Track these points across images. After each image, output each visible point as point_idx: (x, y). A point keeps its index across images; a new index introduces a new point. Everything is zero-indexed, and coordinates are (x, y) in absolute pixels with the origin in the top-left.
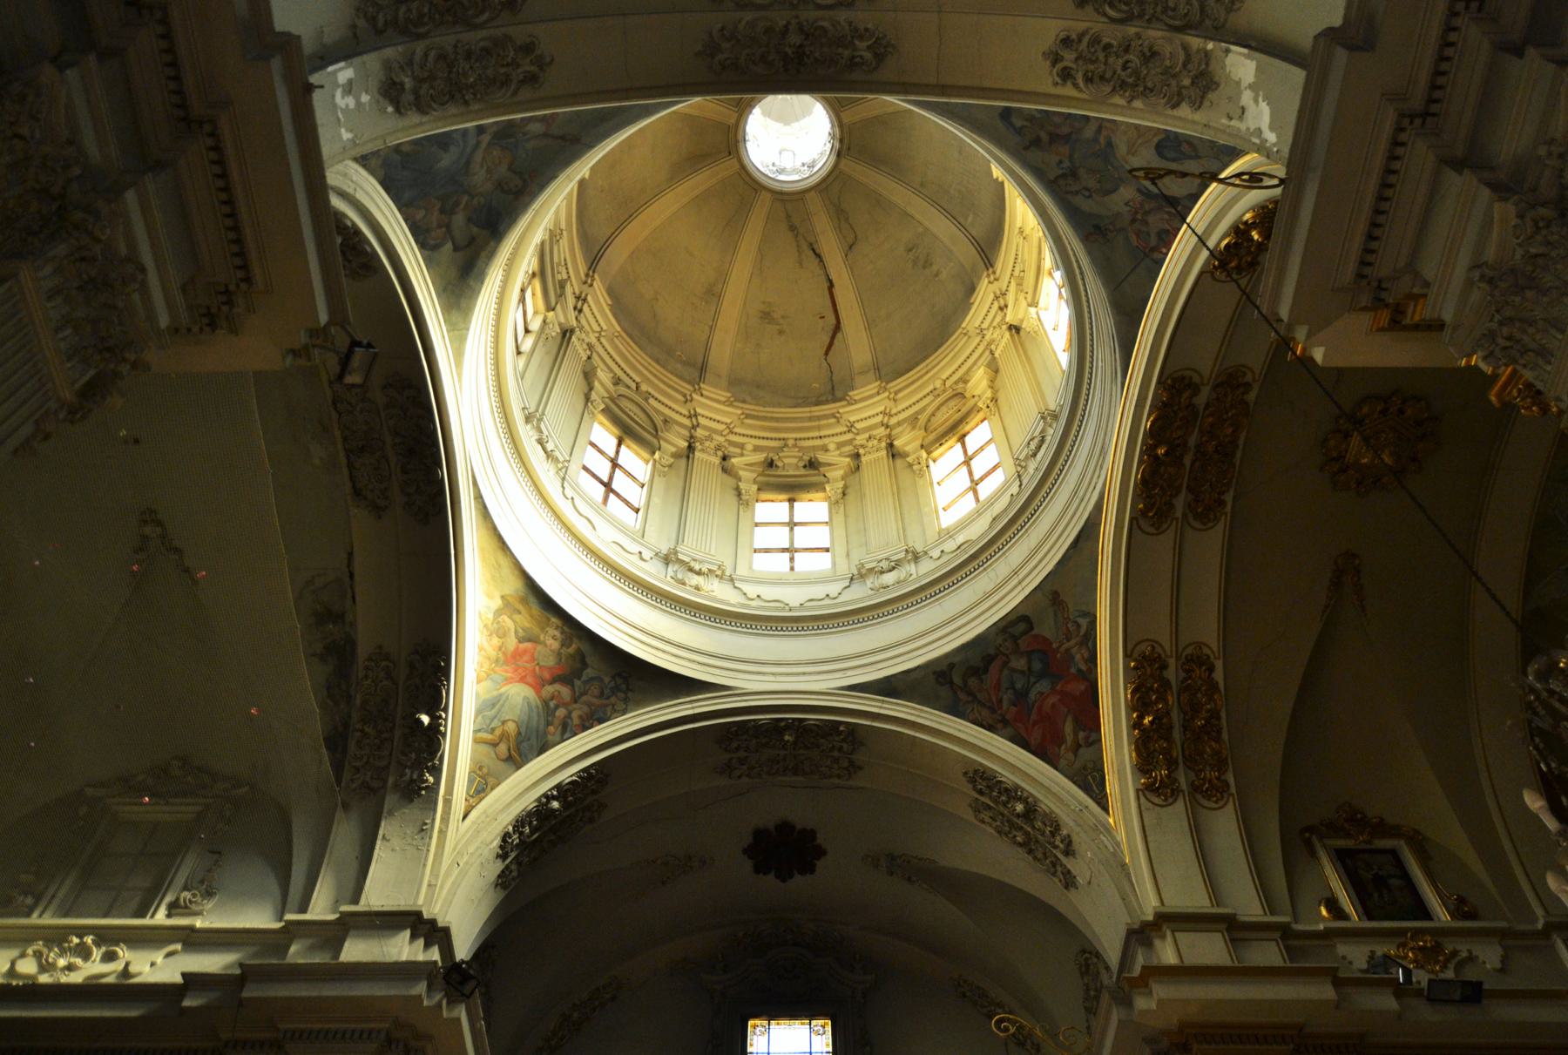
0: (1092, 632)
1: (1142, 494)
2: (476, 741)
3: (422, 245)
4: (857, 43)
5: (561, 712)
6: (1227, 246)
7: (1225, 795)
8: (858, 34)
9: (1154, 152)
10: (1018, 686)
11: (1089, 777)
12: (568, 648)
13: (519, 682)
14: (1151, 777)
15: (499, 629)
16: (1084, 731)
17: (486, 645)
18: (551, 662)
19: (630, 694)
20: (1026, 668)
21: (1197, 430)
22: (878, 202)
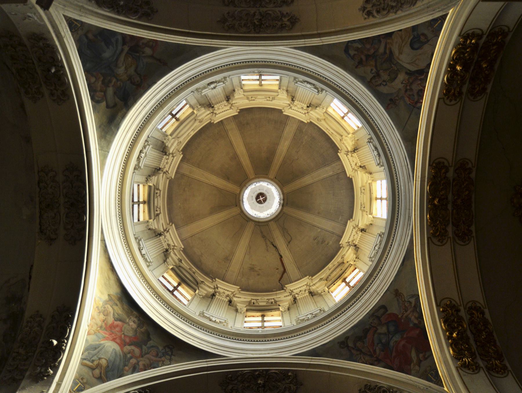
0: (418, 304)
1: (431, 225)
2: (82, 364)
3: (92, 98)
4: (283, 19)
5: (133, 361)
6: (447, 79)
7: (506, 371)
8: (283, 15)
9: (410, 48)
10: (384, 341)
11: (429, 375)
12: (141, 328)
13: (111, 340)
14: (463, 360)
15: (104, 311)
16: (422, 353)
17: (96, 317)
18: (131, 334)
19: (173, 357)
20: (386, 331)
21: (451, 193)
22: (300, 223)
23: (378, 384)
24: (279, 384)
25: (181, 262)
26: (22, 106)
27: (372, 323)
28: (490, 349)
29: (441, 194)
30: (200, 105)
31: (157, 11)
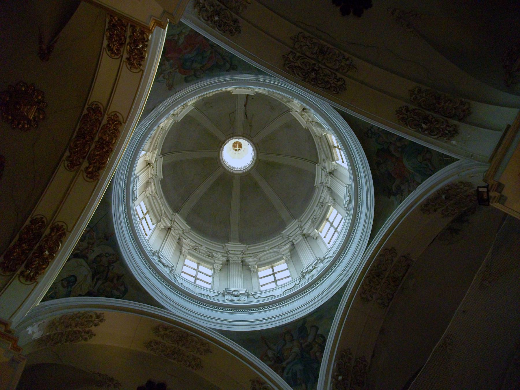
3: (325, 341)
10: (200, 57)
23: (223, 33)
24: (300, 65)
25: (324, 159)
26: (373, 356)
27: (203, 73)
28: (116, 20)
29: (99, 152)
30: (250, 271)
31: (251, 380)
